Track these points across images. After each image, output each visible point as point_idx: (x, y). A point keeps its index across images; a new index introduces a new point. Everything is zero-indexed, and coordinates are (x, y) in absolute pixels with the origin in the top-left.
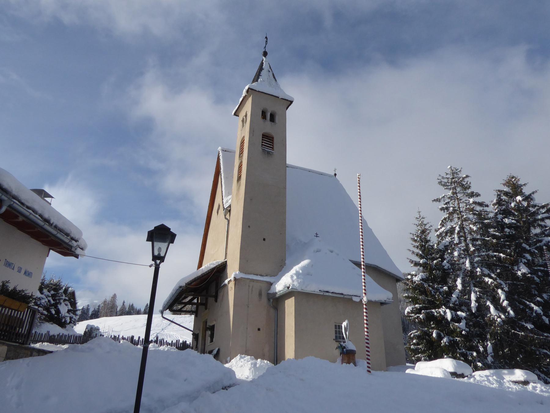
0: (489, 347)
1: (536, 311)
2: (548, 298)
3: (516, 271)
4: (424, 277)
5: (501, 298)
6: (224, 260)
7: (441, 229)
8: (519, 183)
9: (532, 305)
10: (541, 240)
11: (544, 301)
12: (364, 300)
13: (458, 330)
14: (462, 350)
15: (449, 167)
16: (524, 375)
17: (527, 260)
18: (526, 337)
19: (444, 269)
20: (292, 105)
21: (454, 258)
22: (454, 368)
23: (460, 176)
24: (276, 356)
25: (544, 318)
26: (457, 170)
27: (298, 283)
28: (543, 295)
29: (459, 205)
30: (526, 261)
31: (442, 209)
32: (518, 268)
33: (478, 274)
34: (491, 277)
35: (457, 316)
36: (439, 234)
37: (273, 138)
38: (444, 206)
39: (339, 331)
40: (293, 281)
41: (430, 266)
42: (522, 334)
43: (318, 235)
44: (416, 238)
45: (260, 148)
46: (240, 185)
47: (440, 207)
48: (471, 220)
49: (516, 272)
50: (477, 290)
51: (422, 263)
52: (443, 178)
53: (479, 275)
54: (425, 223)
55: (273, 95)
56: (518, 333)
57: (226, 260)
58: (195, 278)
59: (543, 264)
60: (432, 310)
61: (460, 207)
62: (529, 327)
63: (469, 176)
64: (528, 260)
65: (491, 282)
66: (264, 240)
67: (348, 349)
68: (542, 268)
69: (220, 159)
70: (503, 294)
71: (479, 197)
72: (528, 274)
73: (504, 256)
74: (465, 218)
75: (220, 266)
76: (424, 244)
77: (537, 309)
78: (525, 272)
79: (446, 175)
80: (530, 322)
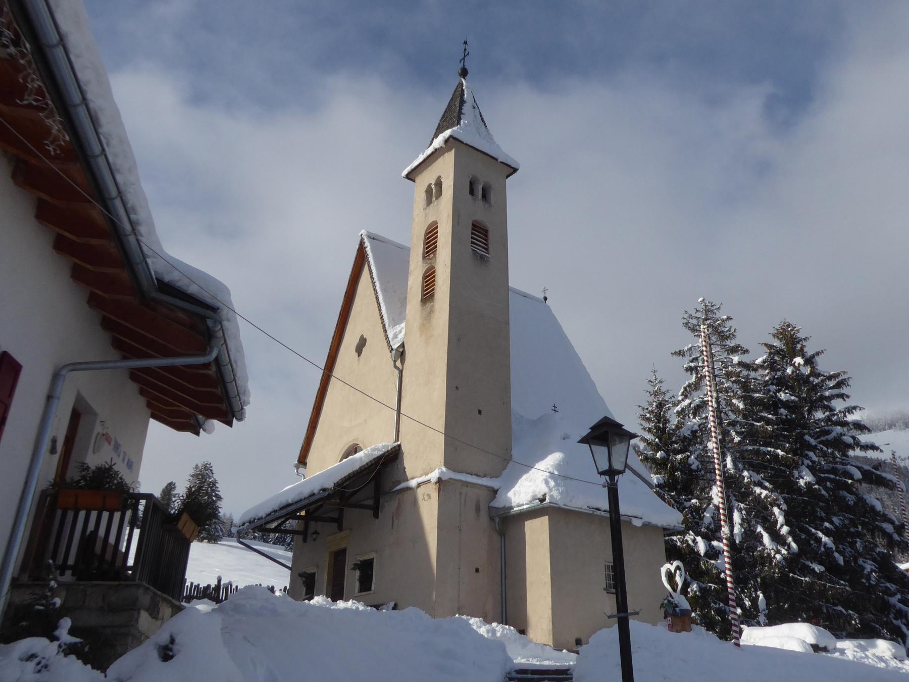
0: (761, 600)
1: (826, 544)
2: (841, 524)
3: (797, 478)
4: (662, 482)
5: (779, 522)
6: (395, 442)
7: (683, 402)
8: (799, 335)
9: (820, 534)
10: (828, 430)
11: (835, 528)
12: (723, 532)
13: (714, 571)
14: (719, 604)
15: (701, 299)
16: (891, 648)
17: (811, 461)
18: (810, 585)
19: (692, 469)
20: (514, 175)
21: (708, 453)
22: (815, 638)
23: (717, 316)
24: (504, 617)
25: (836, 555)
26: (712, 306)
27: (559, 492)
28: (833, 519)
29: (714, 365)
30: (810, 464)
31: (690, 369)
32: (799, 473)
33: (746, 480)
34: (765, 488)
35: (712, 547)
36: (679, 410)
37: (487, 231)
38: (692, 365)
39: (610, 572)
40: (550, 490)
41: (673, 463)
42: (806, 581)
43: (556, 409)
44: (648, 415)
45: (469, 248)
46: (432, 311)
47: (685, 366)
48: (735, 392)
49: (798, 480)
50: (742, 506)
51: (660, 458)
52: (691, 316)
53: (747, 482)
54: (663, 390)
55: (489, 153)
56: (799, 579)
57: (399, 443)
58: (349, 474)
59: (830, 469)
60: (672, 537)
61: (715, 367)
62: (816, 569)
63: (731, 319)
64: (813, 462)
65: (766, 495)
66: (480, 412)
67: (681, 608)
68: (832, 476)
69: (368, 253)
70: (782, 515)
71: (746, 355)
72: (814, 485)
73: (784, 453)
74: (726, 388)
75: (389, 454)
76: (661, 425)
77: (827, 541)
78: (810, 480)
79: (696, 313)
80: (815, 561)
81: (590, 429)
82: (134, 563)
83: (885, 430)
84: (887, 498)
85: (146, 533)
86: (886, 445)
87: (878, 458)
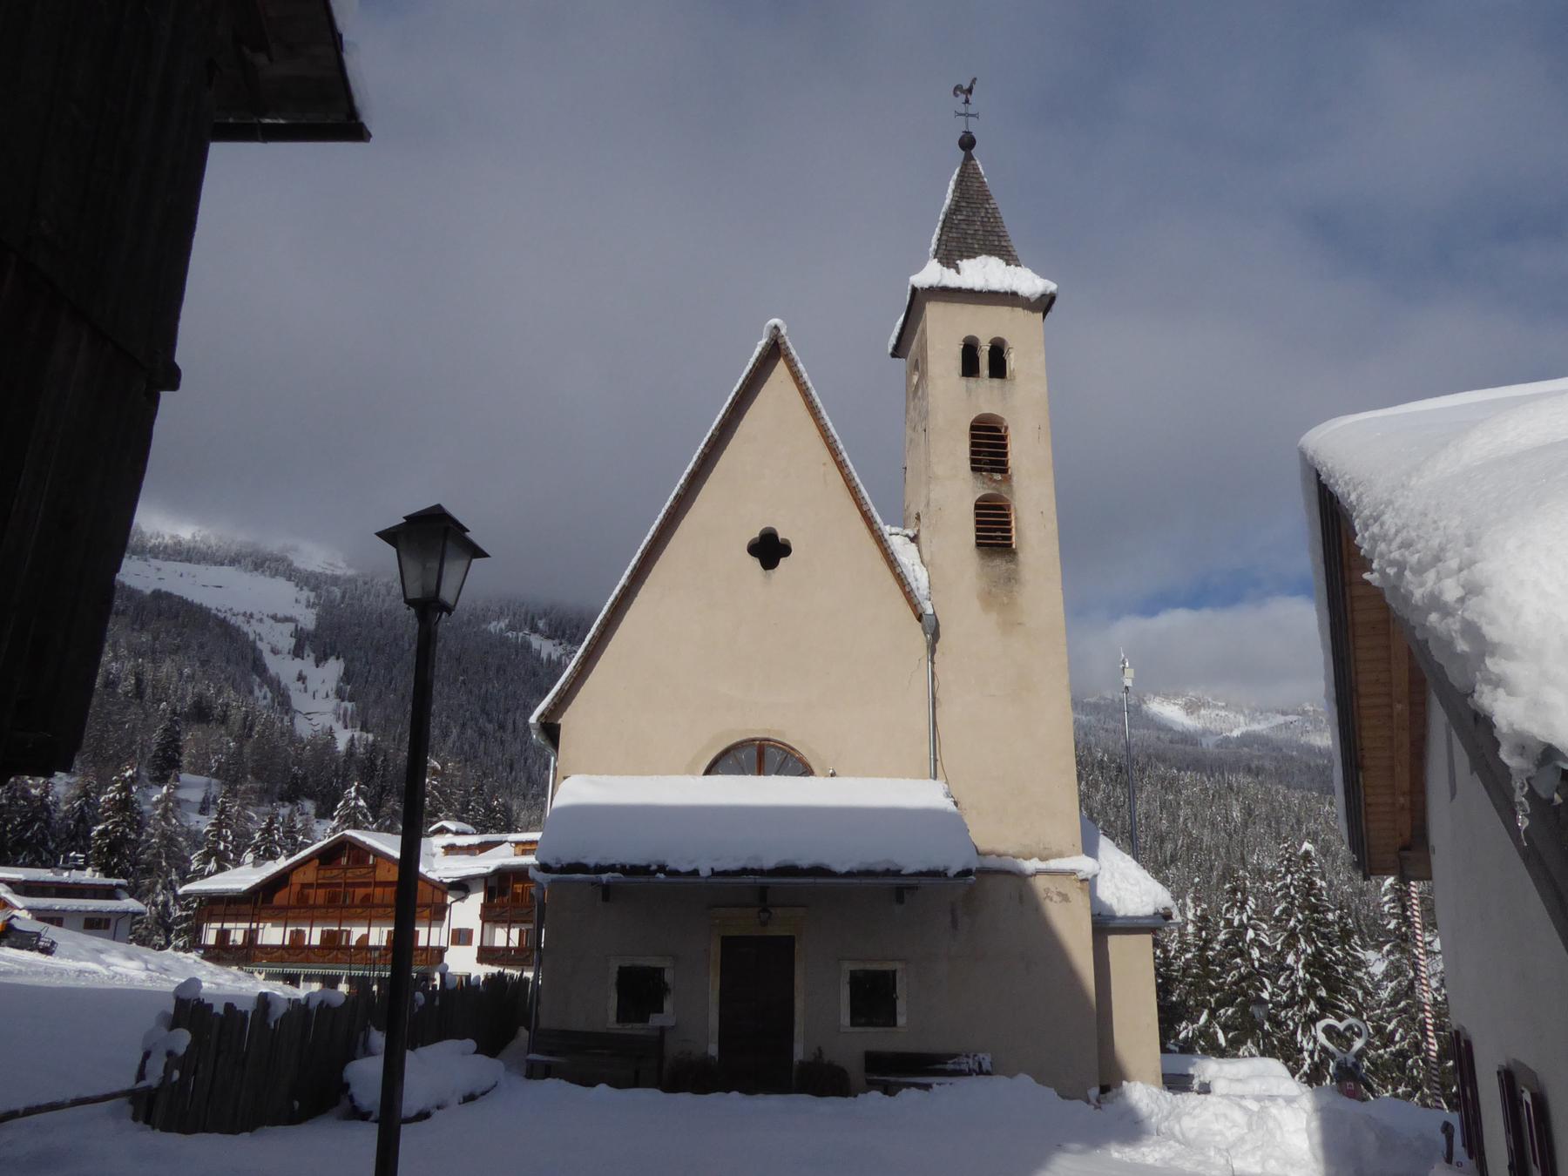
81: (404, 518)
82: (399, 877)
85: (552, 771)
87: (201, 604)
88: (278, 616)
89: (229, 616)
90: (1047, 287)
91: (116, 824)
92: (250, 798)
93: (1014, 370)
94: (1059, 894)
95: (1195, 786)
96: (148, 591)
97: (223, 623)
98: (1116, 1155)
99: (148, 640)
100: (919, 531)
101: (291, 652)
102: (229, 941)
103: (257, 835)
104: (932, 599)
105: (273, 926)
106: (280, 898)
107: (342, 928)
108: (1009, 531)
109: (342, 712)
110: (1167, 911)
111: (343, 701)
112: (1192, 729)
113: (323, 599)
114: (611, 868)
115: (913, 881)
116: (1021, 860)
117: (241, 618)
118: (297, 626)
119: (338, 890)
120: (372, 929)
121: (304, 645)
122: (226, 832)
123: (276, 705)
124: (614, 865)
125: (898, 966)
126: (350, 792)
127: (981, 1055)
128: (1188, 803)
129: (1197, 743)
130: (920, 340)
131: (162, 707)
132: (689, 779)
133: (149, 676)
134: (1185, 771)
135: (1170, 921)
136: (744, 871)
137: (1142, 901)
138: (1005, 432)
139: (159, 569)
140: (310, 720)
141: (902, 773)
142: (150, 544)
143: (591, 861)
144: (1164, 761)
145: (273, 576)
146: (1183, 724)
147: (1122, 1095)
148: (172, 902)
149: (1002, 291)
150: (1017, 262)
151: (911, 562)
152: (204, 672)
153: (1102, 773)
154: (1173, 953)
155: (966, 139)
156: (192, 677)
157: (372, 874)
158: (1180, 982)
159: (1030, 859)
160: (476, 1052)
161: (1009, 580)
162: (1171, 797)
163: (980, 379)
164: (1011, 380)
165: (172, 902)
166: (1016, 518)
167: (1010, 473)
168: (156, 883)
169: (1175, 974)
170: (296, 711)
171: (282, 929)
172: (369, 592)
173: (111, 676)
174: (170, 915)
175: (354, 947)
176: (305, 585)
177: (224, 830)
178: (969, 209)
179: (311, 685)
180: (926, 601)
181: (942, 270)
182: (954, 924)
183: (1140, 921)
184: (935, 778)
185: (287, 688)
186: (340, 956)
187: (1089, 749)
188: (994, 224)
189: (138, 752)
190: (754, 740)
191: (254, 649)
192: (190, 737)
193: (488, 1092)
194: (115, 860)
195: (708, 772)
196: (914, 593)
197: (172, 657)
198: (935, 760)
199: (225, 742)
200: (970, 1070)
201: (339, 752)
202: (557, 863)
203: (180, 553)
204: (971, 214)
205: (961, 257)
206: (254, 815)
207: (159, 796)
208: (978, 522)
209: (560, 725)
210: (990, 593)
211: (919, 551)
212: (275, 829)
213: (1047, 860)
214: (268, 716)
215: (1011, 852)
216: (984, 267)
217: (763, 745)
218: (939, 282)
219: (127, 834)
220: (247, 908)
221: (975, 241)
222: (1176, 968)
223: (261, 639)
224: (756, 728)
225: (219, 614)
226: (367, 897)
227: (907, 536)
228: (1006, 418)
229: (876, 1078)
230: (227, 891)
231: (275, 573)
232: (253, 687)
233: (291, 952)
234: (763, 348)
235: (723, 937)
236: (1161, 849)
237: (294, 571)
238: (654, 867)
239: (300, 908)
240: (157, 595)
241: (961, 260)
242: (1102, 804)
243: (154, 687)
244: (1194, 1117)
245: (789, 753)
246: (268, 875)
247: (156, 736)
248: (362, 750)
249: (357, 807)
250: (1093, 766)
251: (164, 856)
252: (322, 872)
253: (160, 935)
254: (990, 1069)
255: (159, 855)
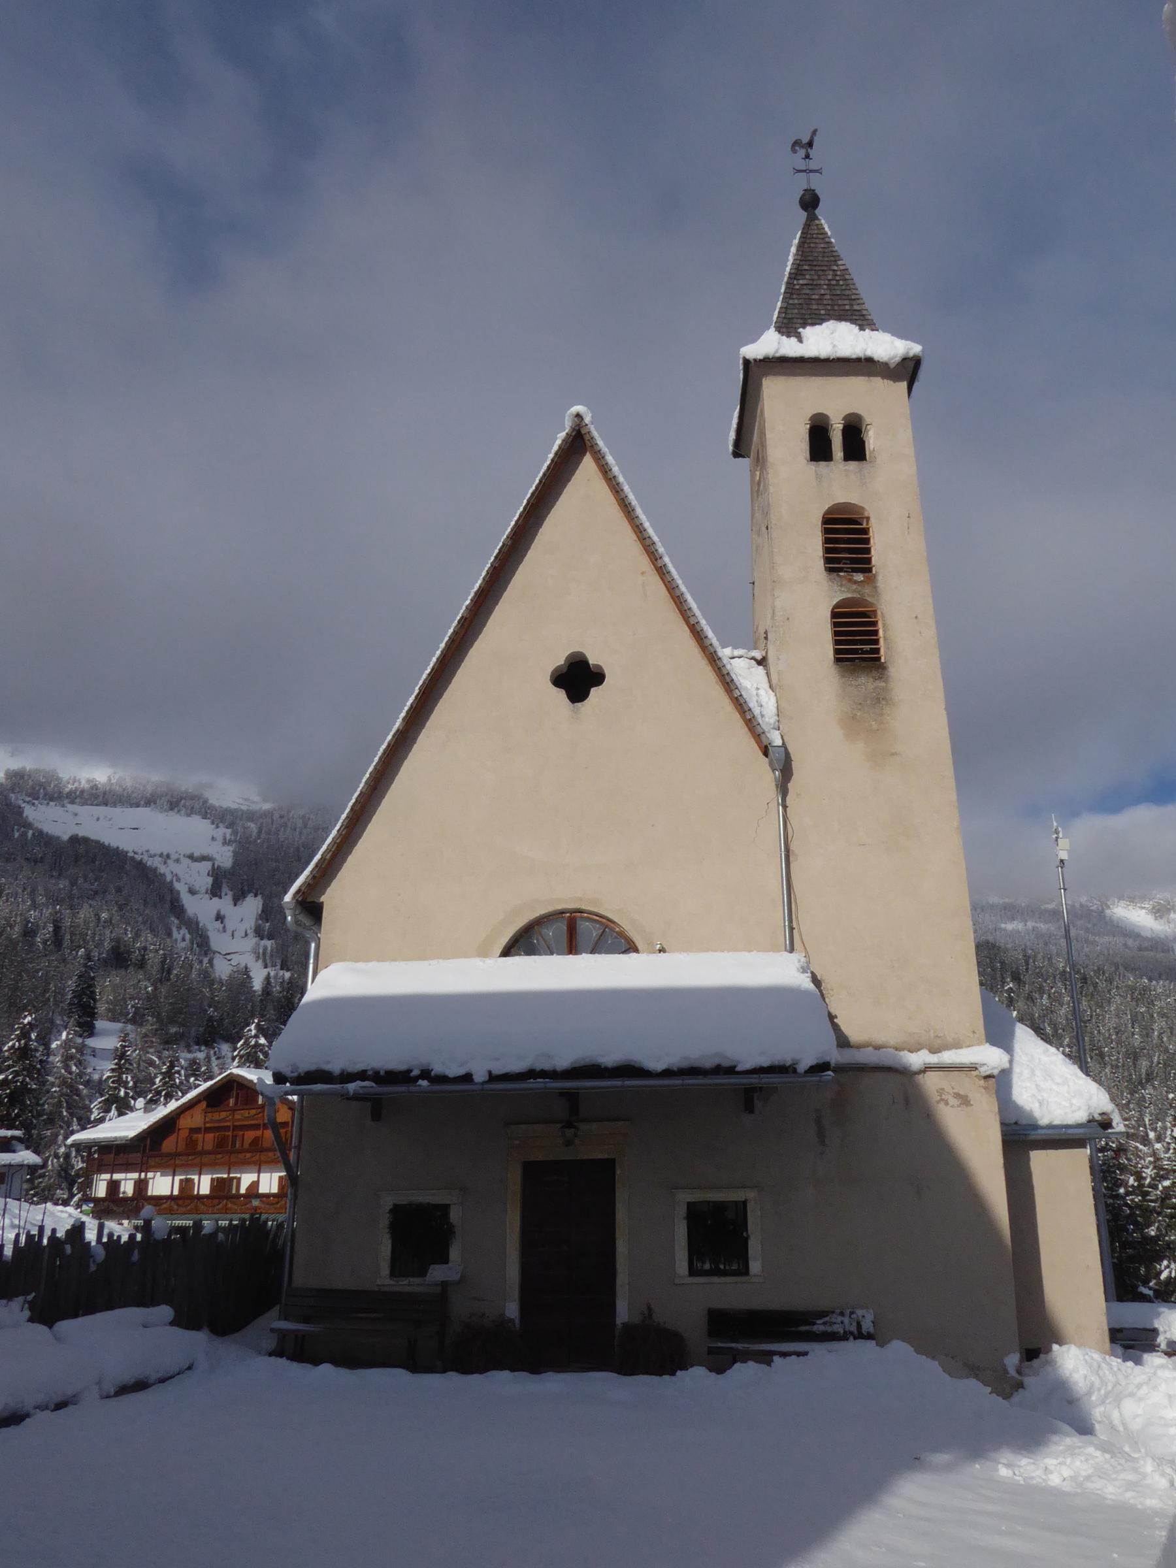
83: (138, 806)
84: (116, 911)
85: (311, 961)
86: (134, 829)
87: (118, 848)
88: (195, 855)
89: (145, 858)
90: (909, 349)
91: (16, 1074)
92: (152, 1042)
93: (874, 450)
94: (957, 1096)
95: (1168, 996)
96: (66, 837)
97: (140, 865)
98: (1004, 1472)
99: (65, 886)
100: (767, 652)
101: (209, 892)
102: (118, 1192)
103: (158, 1080)
104: (781, 728)
105: (161, 1175)
106: (168, 1145)
107: (231, 1175)
108: (877, 642)
109: (261, 951)
110: (1105, 1117)
111: (262, 939)
112: (1162, 936)
113: (239, 836)
114: (362, 1075)
115: (753, 1080)
116: (906, 1052)
117: (158, 860)
118: (213, 865)
119: (227, 1133)
120: (261, 1175)
121: (221, 882)
122: (127, 1077)
123: (195, 946)
124: (364, 1072)
125: (750, 1195)
126: (250, 1030)
127: (860, 1312)
128: (1163, 1015)
129: (1169, 950)
130: (760, 424)
131: (80, 953)
132: (477, 962)
133: (67, 922)
134: (1156, 981)
135: (1110, 1131)
136: (531, 1074)
137: (1072, 1105)
138: (867, 524)
139: (76, 815)
140: (229, 960)
141: (749, 946)
142: (67, 790)
143: (335, 1067)
144: (1133, 970)
145: (189, 815)
146: (1151, 929)
147: (1051, 1363)
148: (74, 1154)
149: (854, 356)
150: (873, 327)
151: (755, 686)
152: (122, 917)
153: (1065, 985)
154: (1148, 1180)
155: (807, 197)
156: (109, 922)
157: (261, 1114)
158: (1159, 1214)
159: (919, 1050)
160: (172, 1324)
161: (878, 701)
162: (1143, 1010)
163: (832, 462)
164: (871, 462)
165: (74, 1154)
166: (884, 625)
167: (874, 572)
168: (57, 1135)
169: (1153, 1204)
170: (214, 952)
171: (171, 1178)
172: (285, 825)
173: (30, 925)
174: (73, 1167)
175: (243, 1196)
176: (221, 822)
177: (124, 1076)
178: (813, 272)
179: (230, 924)
180: (772, 731)
181: (780, 339)
182: (821, 1135)
183: (1070, 1131)
184: (792, 950)
185: (205, 930)
186: (230, 1205)
187: (1050, 959)
188: (844, 287)
189: (52, 1000)
190: (562, 912)
191: (171, 889)
192: (108, 986)
193: (172, 1377)
194: (16, 1111)
195: (506, 953)
196: (756, 720)
197: (90, 902)
198: (792, 929)
199: (143, 987)
200: (845, 1332)
201: (255, 991)
202: (292, 1072)
203: (96, 797)
204: (816, 277)
205: (804, 326)
206: (156, 1059)
207: (58, 1043)
208: (836, 634)
209: (322, 903)
210: (854, 717)
211: (768, 674)
212: (175, 1073)
213: (940, 1051)
214: (186, 958)
215: (892, 1043)
216: (832, 333)
217: (574, 916)
218: (777, 351)
219: (27, 1084)
220: (136, 1157)
221: (820, 307)
222: (1153, 1198)
223: (178, 880)
224: (563, 897)
225: (136, 856)
226: (256, 1141)
227: (753, 658)
228: (866, 507)
229: (720, 1345)
230: (116, 1139)
231: (191, 812)
232: (171, 929)
233: (180, 1202)
234: (563, 441)
235: (525, 1162)
236: (1135, 1067)
237: (209, 808)
238: (416, 1072)
239: (188, 1155)
240: (75, 840)
241: (804, 328)
242: (1067, 1019)
243: (72, 934)
244: (1141, 1399)
245: (607, 926)
246: (155, 1120)
247: (71, 983)
248: (278, 988)
249: (257, 1045)
250: (1055, 977)
251: (65, 1105)
252: (209, 1115)
253: (62, 1189)
254: (871, 1330)
255: (59, 1104)
